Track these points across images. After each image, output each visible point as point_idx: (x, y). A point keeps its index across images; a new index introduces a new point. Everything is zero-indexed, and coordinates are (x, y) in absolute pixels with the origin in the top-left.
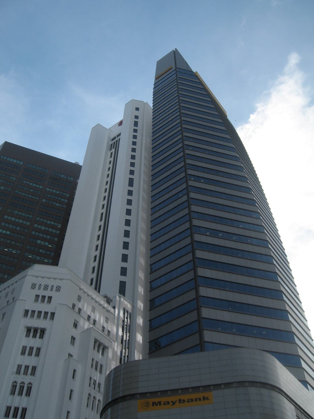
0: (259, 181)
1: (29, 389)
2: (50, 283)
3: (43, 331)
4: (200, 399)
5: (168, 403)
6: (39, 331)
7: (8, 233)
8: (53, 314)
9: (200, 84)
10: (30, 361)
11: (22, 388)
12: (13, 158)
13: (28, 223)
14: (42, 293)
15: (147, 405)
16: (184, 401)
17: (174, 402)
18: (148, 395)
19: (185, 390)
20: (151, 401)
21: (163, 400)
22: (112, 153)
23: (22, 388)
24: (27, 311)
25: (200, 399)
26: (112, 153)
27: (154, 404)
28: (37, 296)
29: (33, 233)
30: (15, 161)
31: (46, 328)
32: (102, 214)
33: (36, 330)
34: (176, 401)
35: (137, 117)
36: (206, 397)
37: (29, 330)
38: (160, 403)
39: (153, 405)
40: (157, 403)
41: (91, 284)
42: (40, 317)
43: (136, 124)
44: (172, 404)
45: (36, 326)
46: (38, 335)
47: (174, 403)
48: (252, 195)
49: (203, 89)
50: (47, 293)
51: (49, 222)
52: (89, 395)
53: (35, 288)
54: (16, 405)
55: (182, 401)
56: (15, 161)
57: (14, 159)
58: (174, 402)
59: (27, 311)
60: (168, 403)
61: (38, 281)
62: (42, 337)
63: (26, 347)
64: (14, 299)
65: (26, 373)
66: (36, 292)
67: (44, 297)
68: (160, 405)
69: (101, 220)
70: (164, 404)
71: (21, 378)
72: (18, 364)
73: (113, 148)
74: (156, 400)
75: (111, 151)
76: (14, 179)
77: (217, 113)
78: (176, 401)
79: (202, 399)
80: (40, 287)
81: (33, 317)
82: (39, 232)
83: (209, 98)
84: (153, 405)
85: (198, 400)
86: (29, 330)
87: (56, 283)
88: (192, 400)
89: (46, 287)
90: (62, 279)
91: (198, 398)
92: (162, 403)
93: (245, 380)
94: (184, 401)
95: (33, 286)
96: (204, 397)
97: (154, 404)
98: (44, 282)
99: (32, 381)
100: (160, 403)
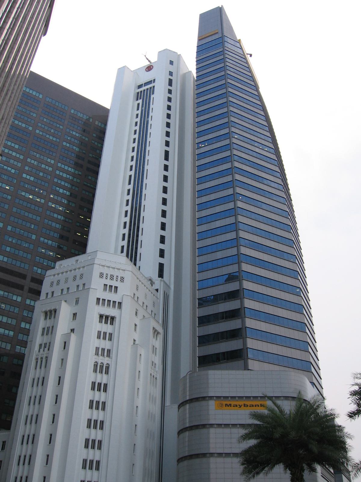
0: (288, 187)
1: (108, 368)
2: (116, 273)
3: (113, 318)
4: (258, 406)
5: (236, 406)
6: (110, 318)
7: (32, 179)
8: (120, 303)
9: (251, 79)
10: (106, 344)
11: (101, 367)
12: (32, 90)
13: (50, 169)
14: (109, 282)
15: (222, 405)
16: (247, 406)
17: (241, 405)
18: (222, 398)
19: (248, 398)
20: (224, 403)
21: (233, 403)
22: (138, 104)
23: (101, 367)
24: (98, 299)
25: (258, 406)
26: (138, 104)
27: (226, 405)
28: (105, 285)
29: (56, 180)
30: (34, 93)
31: (116, 316)
32: (130, 176)
33: (107, 317)
34: (242, 405)
35: (171, 74)
36: (262, 405)
37: (101, 316)
38: (230, 405)
39: (226, 406)
40: (228, 404)
41: (122, 252)
42: (110, 305)
43: (170, 83)
44: (239, 407)
45: (107, 313)
46: (109, 322)
47: (240, 406)
48: (289, 220)
49: (255, 86)
50: (114, 283)
51: (66, 168)
52: (151, 374)
53: (103, 277)
54: (100, 382)
55: (246, 406)
56: (34, 93)
57: (33, 90)
58: (241, 405)
59: (98, 299)
60: (236, 406)
61: (105, 271)
62: (112, 323)
63: (101, 332)
64: (84, 285)
65: (103, 355)
66: (104, 281)
67: (111, 286)
68: (231, 406)
69: (130, 184)
70: (234, 406)
71: (101, 360)
72: (96, 346)
73: (140, 99)
74: (228, 403)
75: (138, 102)
76: (35, 115)
77: (269, 133)
78: (242, 405)
79: (260, 406)
80: (107, 276)
81: (104, 306)
82: (61, 180)
83: (263, 111)
84: (226, 406)
85: (257, 406)
86: (101, 316)
87: (120, 274)
88: (253, 406)
89: (112, 278)
90: (125, 270)
91: (257, 405)
92: (232, 405)
93: (290, 396)
94: (247, 406)
95: (101, 275)
96: (261, 404)
97: (226, 405)
98: (110, 272)
99: (109, 362)
100: (230, 405)
